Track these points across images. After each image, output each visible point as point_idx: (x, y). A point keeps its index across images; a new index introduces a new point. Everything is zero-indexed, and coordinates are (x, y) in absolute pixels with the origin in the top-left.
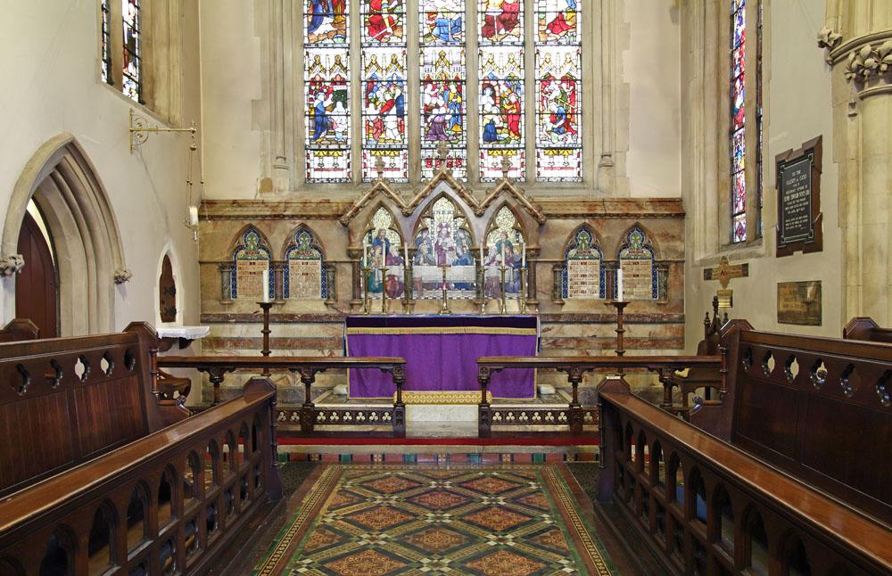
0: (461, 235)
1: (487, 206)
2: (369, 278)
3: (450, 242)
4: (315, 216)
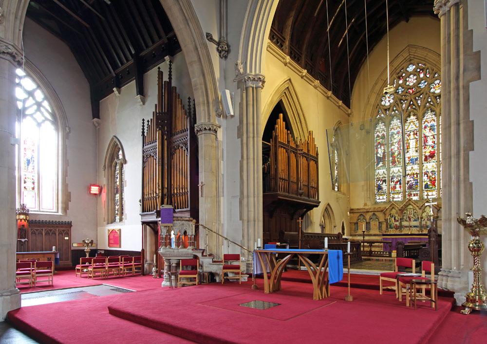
2: (390, 226)
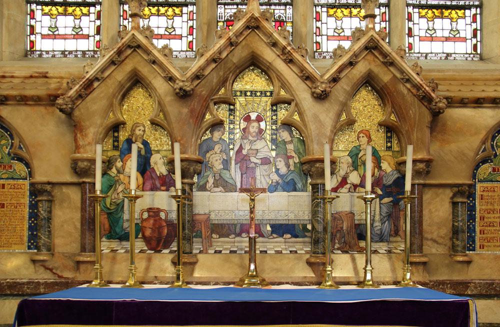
0: (285, 135)
1: (335, 80)
2: (114, 214)
3: (107, 275)
4: (14, 98)
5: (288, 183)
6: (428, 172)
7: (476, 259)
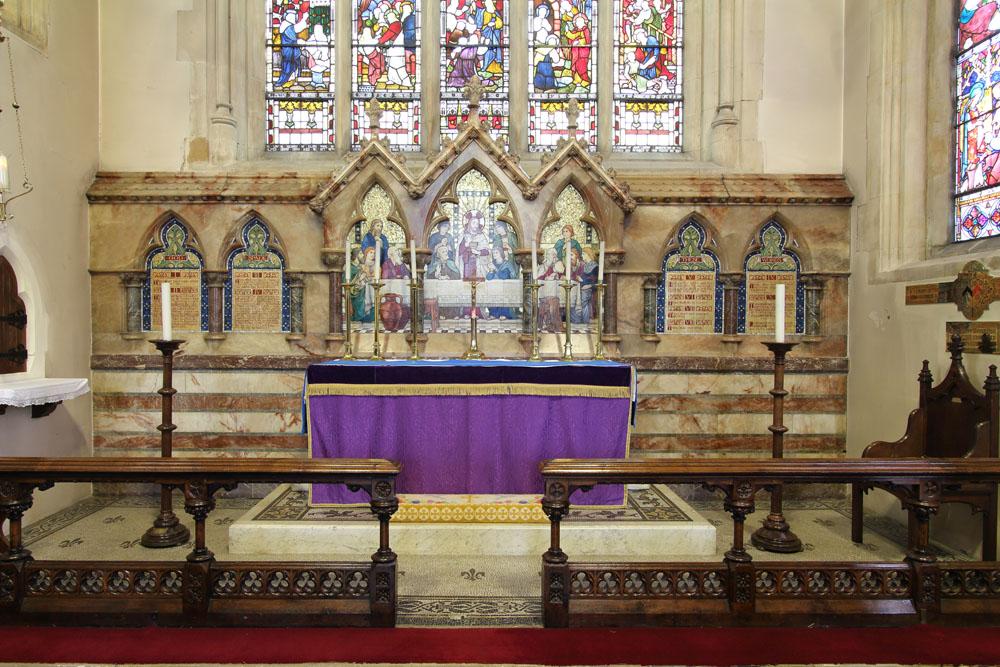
0: (501, 230)
1: (542, 183)
2: (356, 300)
4: (271, 198)
5: (503, 272)
6: (621, 263)
7: (663, 339)
